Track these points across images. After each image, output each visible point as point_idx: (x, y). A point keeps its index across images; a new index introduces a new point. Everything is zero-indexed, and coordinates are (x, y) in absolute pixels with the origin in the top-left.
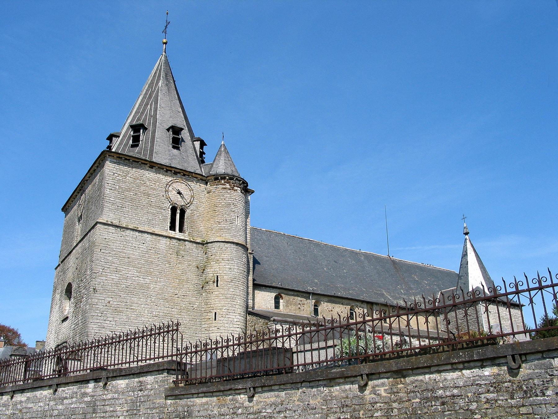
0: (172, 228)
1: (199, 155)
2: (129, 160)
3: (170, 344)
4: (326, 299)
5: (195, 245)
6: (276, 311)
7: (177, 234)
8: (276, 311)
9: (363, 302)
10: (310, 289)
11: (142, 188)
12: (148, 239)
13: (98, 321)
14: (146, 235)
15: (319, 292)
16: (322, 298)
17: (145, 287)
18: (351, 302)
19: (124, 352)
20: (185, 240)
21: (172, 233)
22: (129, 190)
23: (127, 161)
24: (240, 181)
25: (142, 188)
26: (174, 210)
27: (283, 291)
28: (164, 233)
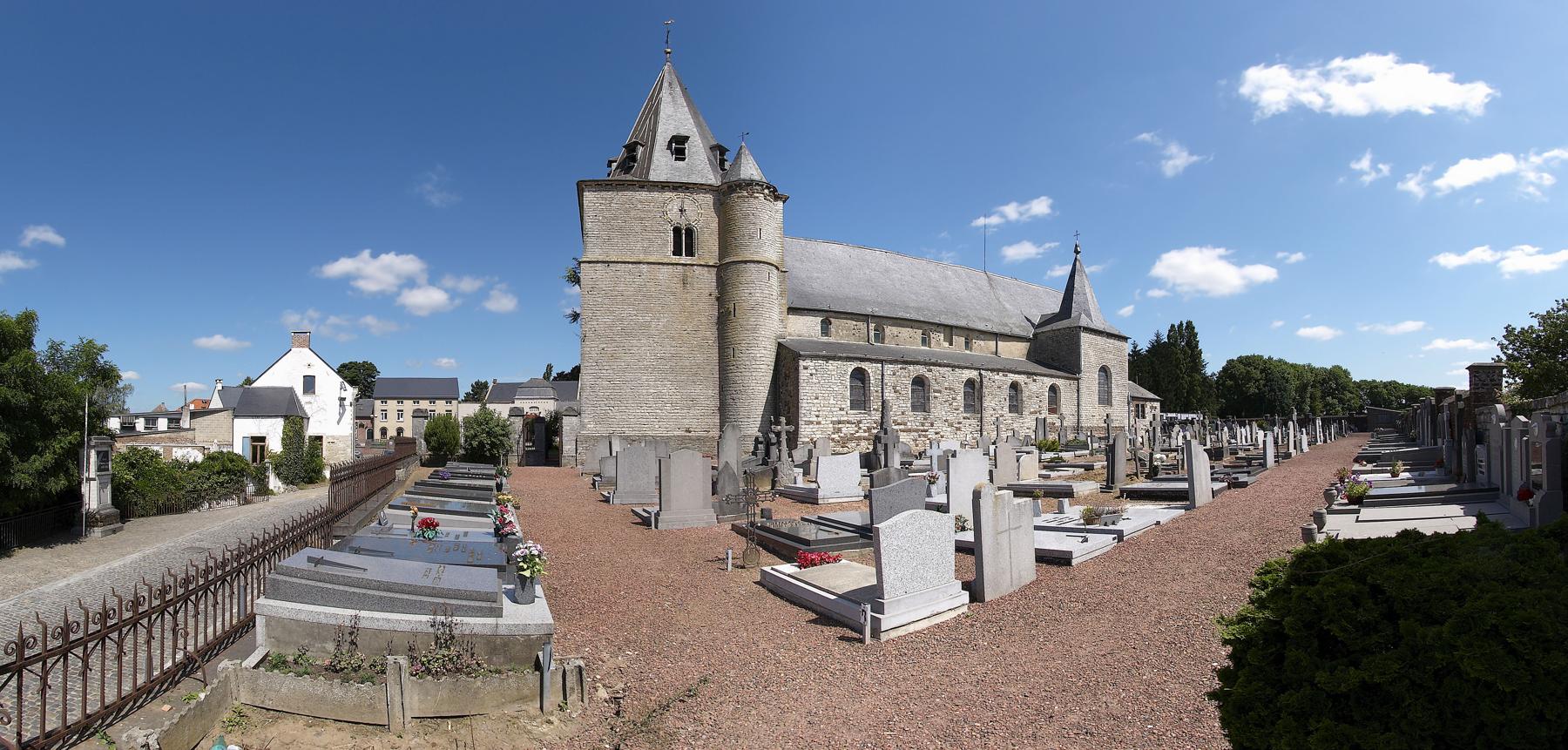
0: (677, 252)
1: (136, 556)
2: (611, 185)
3: (169, 643)
4: (891, 322)
5: (706, 269)
6: (825, 339)
7: (684, 259)
8: (825, 339)
9: (939, 325)
10: (869, 310)
11: (633, 213)
12: (645, 270)
13: (593, 371)
14: (642, 266)
15: (881, 314)
16: (885, 321)
17: (647, 326)
18: (923, 325)
19: (235, 601)
20: (693, 265)
21: (676, 259)
22: (615, 218)
23: (610, 187)
24: (762, 185)
25: (633, 213)
26: (677, 231)
27: (830, 314)
28: (665, 261)
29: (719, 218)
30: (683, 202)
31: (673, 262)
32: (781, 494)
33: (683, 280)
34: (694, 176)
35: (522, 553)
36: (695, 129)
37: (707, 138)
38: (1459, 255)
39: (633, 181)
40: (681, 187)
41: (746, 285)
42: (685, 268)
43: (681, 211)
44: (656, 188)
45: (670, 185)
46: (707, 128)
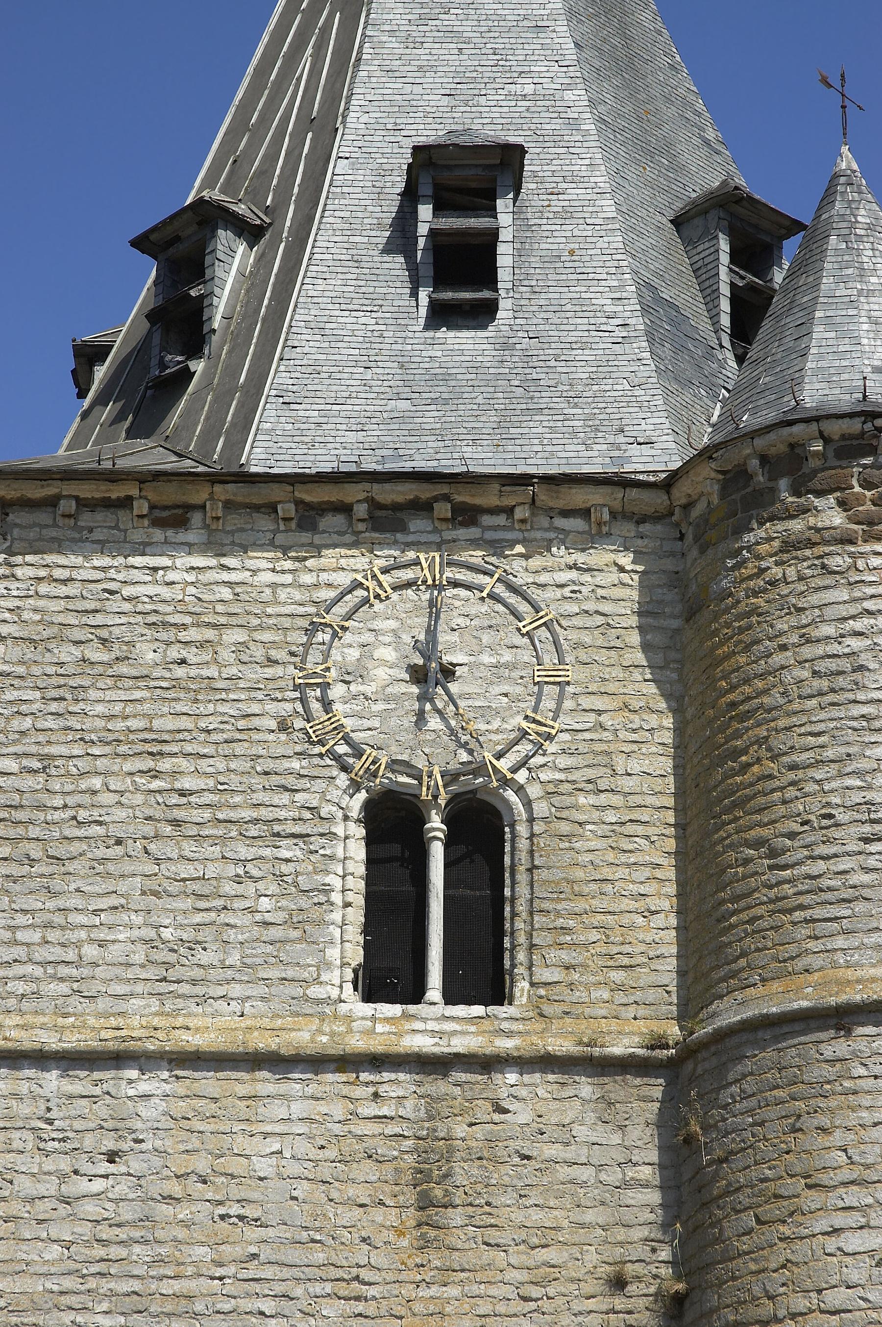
2: (52, 502)
5: (586, 1087)
12: (149, 1111)
29: (677, 710)
30: (434, 609)
31: (357, 1043)
32: (824, 732)
33: (421, 1176)
34: (538, 426)
35: (385, 1040)
36: (577, 97)
37: (667, 148)
38: (484, 327)
39: (114, 477)
40: (422, 507)
41: (853, 1196)
42: (439, 1086)
43: (418, 675)
44: (265, 523)
45: (353, 493)
46: (685, 84)
